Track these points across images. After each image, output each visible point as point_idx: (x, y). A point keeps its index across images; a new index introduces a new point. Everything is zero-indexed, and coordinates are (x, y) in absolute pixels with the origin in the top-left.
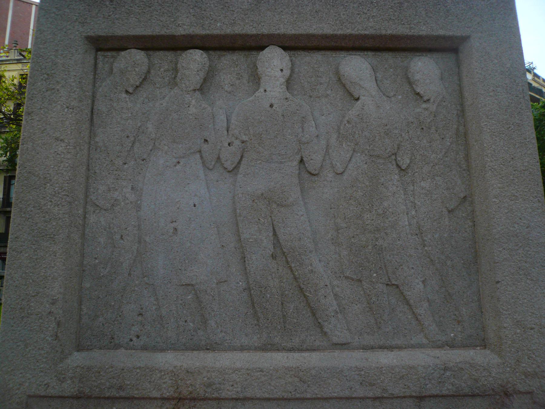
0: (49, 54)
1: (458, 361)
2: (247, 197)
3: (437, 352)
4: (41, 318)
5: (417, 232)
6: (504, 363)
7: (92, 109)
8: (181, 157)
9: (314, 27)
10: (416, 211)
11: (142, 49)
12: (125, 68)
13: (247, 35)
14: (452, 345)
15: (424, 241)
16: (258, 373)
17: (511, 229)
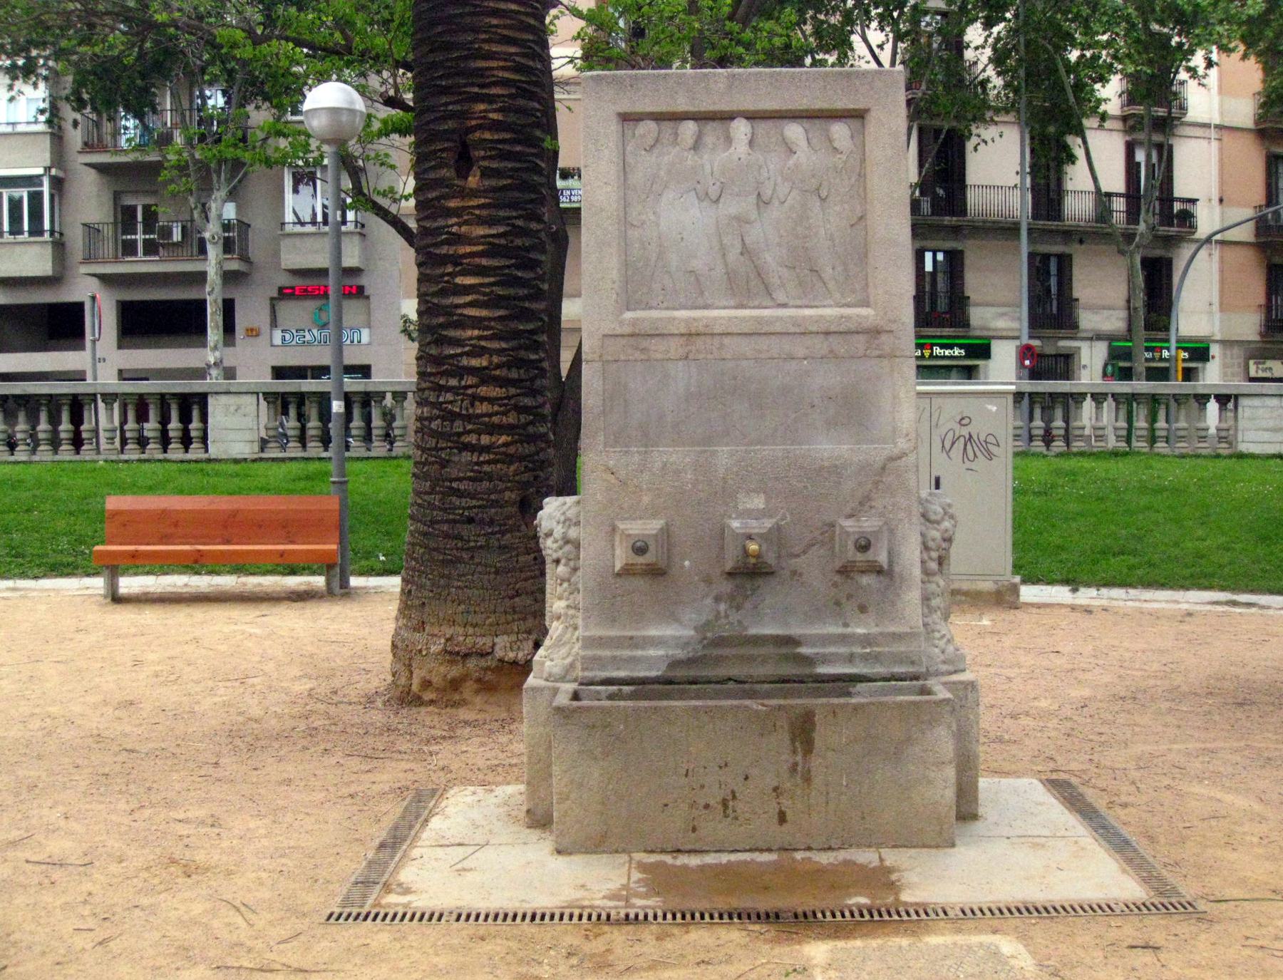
14: (848, 305)
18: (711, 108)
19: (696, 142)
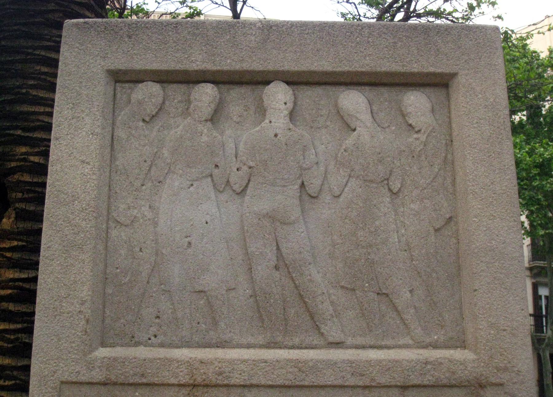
0: (74, 85)
1: (438, 357)
2: (254, 216)
3: (421, 351)
4: (71, 316)
5: (406, 248)
6: (479, 359)
7: (113, 136)
8: (194, 180)
9: (315, 64)
10: (405, 230)
11: (157, 82)
12: (142, 99)
13: (253, 72)
14: (435, 346)
15: (412, 256)
16: (263, 364)
17: (489, 244)
18: (238, 67)
19: (216, 111)
